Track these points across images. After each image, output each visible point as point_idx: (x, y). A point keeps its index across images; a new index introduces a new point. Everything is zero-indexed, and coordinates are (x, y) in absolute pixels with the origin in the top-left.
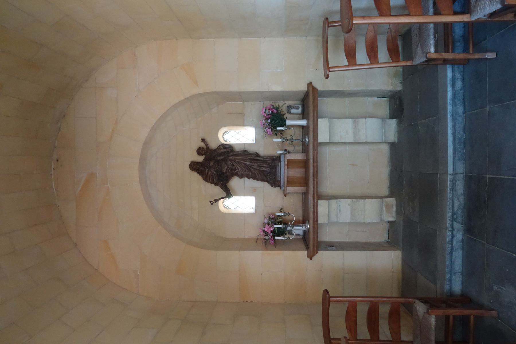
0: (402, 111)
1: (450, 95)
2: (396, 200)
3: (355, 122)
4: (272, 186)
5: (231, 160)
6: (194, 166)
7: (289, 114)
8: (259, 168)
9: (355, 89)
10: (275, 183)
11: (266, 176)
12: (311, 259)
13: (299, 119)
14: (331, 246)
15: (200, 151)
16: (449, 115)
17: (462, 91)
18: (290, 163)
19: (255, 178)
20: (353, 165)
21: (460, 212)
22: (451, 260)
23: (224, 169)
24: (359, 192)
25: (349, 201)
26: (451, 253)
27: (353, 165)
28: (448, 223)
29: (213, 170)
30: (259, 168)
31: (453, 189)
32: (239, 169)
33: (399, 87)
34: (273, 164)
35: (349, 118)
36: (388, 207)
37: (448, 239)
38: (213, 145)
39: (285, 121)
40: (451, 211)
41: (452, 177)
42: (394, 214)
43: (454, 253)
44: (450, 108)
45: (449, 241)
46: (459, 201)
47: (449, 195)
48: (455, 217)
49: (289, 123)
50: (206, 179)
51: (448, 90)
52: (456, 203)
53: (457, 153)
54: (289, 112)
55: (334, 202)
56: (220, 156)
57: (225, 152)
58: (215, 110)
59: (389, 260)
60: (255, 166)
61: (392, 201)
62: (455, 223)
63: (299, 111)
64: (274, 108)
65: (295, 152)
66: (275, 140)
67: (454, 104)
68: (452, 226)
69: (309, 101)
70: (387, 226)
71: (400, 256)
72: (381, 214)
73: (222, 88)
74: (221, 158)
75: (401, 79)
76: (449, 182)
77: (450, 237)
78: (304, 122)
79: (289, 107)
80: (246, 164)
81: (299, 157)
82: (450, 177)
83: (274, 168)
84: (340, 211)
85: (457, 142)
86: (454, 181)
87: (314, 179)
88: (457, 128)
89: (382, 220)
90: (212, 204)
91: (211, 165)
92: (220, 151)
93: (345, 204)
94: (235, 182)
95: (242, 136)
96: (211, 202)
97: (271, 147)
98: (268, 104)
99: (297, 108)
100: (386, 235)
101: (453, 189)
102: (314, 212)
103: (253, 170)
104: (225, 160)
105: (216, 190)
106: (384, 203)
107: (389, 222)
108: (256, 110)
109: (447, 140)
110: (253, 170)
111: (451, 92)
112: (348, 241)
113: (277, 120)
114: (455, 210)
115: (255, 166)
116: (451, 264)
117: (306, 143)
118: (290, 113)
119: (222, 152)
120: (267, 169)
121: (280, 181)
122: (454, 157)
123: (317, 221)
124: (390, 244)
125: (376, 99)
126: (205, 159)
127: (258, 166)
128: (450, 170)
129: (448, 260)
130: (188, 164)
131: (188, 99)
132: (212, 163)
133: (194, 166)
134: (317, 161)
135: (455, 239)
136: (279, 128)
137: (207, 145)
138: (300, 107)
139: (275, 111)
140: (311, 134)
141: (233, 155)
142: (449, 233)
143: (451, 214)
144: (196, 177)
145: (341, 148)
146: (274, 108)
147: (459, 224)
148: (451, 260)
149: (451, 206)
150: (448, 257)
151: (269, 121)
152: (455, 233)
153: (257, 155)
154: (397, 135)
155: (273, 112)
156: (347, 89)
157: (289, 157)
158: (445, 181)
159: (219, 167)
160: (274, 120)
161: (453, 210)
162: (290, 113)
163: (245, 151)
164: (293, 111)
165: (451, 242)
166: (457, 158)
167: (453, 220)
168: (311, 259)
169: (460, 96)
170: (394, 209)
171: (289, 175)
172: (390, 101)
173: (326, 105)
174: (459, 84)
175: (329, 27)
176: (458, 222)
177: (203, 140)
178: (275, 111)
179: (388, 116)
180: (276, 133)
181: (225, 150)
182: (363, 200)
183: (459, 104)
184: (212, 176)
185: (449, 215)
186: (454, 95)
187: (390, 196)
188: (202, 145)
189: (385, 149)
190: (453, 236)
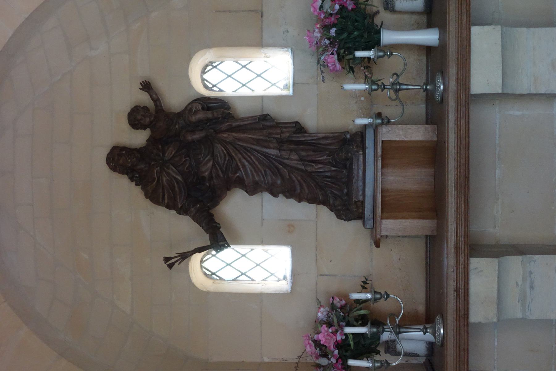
4: (339, 217)
5: (224, 143)
6: (120, 159)
10: (347, 208)
13: (418, 27)
15: (137, 116)
18: (391, 153)
19: (291, 193)
23: (206, 169)
29: (172, 171)
32: (247, 169)
34: (343, 155)
38: (175, 101)
39: (378, 32)
49: (388, 37)
55: (514, 263)
56: (193, 132)
57: (208, 120)
60: (293, 159)
66: (349, 87)
74: (197, 136)
81: (417, 134)
84: (532, 287)
87: (458, 197)
90: (171, 266)
91: (168, 156)
92: (194, 119)
94: (236, 206)
96: (167, 259)
102: (457, 290)
105: (183, 228)
110: (285, 172)
113: (357, 29)
115: (293, 159)
117: (438, 96)
120: (327, 168)
121: (363, 203)
123: (466, 315)
126: (151, 141)
127: (301, 159)
130: (103, 153)
132: (170, 152)
133: (120, 159)
134: (467, 147)
136: (359, 54)
137: (156, 100)
140: (452, 70)
141: (231, 129)
151: (333, 31)
153: (298, 127)
157: (388, 134)
171: (389, 186)
177: (147, 86)
180: (351, 67)
181: (209, 115)
188: (144, 99)
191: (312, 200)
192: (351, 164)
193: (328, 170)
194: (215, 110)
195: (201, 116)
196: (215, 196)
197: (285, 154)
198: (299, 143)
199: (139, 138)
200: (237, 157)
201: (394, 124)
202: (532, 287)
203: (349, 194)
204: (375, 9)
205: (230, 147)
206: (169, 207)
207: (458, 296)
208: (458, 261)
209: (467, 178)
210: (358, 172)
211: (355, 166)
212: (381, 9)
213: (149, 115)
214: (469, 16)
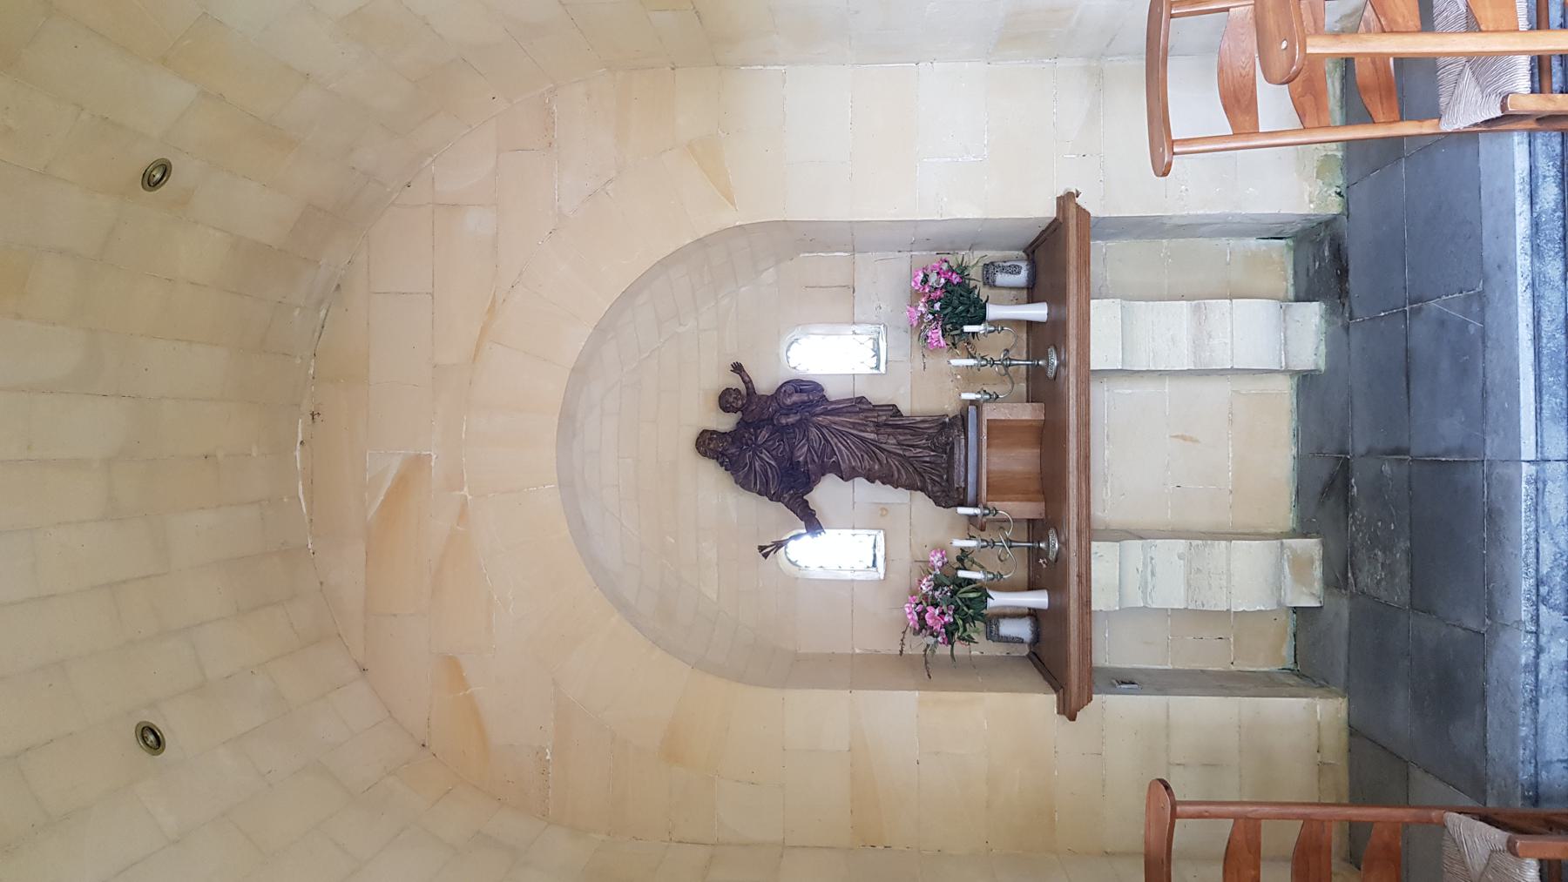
0: (1343, 274)
1: (1522, 225)
2: (1324, 545)
3: (1197, 309)
4: (938, 504)
5: (819, 427)
6: (708, 444)
7: (1020, 289)
8: (916, 453)
9: (1201, 212)
10: (947, 494)
11: (920, 474)
12: (1072, 718)
13: (1018, 302)
14: (1125, 681)
15: (726, 401)
16: (1522, 284)
17: (1559, 214)
18: (1001, 432)
19: (888, 479)
20: (1184, 438)
21: (1558, 576)
22: (1535, 721)
23: (801, 454)
24: (1202, 518)
25: (1181, 545)
26: (1535, 701)
27: (1184, 438)
28: (1525, 612)
29: (765, 456)
30: (916, 453)
31: (1537, 507)
32: (843, 453)
33: (1334, 207)
34: (943, 439)
35: (1182, 298)
36: (1300, 566)
37: (1525, 658)
38: (765, 383)
39: (984, 307)
40: (1532, 571)
41: (1533, 469)
42: (1317, 586)
43: (1541, 701)
44: (1523, 262)
45: (1526, 665)
46: (1556, 544)
47: (1525, 525)
48: (1544, 590)
49: (993, 312)
50: (745, 484)
51: (1518, 211)
52: (1547, 549)
53: (1546, 398)
54: (989, 282)
55: (1134, 546)
56: (787, 415)
57: (804, 402)
58: (769, 276)
59: (1308, 720)
60: (891, 443)
61: (1311, 547)
62: (1543, 609)
63: (1021, 278)
64: (951, 269)
65: (1012, 399)
66: (955, 362)
67: (1536, 252)
68: (1536, 619)
69: (1052, 255)
70: (1289, 623)
71: (1343, 714)
72: (1278, 587)
73: (802, 209)
74: (792, 419)
75: (1340, 182)
76: (1524, 485)
77: (1532, 653)
78: (1038, 312)
79: (989, 269)
80: (863, 440)
81: (1027, 413)
82: (1527, 470)
83: (948, 450)
84: (1153, 574)
85: (1545, 365)
86: (1539, 483)
87: (1079, 477)
88: (1544, 325)
89: (1279, 603)
90: (766, 556)
91: (760, 440)
92: (788, 401)
93: (1169, 552)
94: (827, 493)
95: (843, 353)
96: (761, 548)
97: (923, 384)
98: (931, 259)
99: (1015, 270)
100: (1287, 651)
101: (1537, 507)
102: (1079, 576)
103: (882, 456)
104: (802, 425)
105: (770, 515)
106: (1287, 552)
107: (1295, 610)
108: (888, 283)
109: (1516, 359)
110: (882, 456)
111: (1527, 214)
112: (1170, 667)
113: (961, 303)
114: (1544, 570)
115: (891, 443)
116: (1536, 734)
117: (1051, 373)
118: (993, 286)
119: (795, 403)
120: (926, 453)
121: (965, 489)
122: (1539, 412)
123: (1089, 603)
124: (1305, 673)
125: (1253, 242)
126: (742, 424)
127: (899, 444)
128: (1528, 450)
129: (1527, 721)
130: (691, 435)
131: (701, 243)
132: (764, 435)
133: (708, 444)
134: (1087, 425)
135: (1544, 657)
136: (967, 328)
137: (748, 383)
138: (1024, 265)
139: (956, 279)
140: (1072, 345)
141: (826, 413)
142: (1527, 641)
143: (1532, 581)
144: (711, 479)
145: (1146, 389)
146: (951, 269)
147: (1556, 614)
148: (1535, 721)
149: (1531, 559)
150: (1524, 715)
151: (937, 306)
152: (1543, 640)
153: (894, 410)
154: (1323, 348)
155: (948, 281)
156: (1179, 213)
157: (991, 412)
158: (1510, 486)
159: (777, 444)
160: (953, 306)
161: (1537, 570)
162: (993, 286)
163: (861, 400)
164: (1002, 279)
165: (1535, 667)
166: (1546, 413)
167: (1539, 600)
168: (1072, 718)
169: (1553, 229)
170: (1317, 572)
171: (992, 468)
172: (1295, 250)
173: (1108, 259)
174: (1550, 193)
175: (1172, 16)
176: (1554, 608)
177: (738, 368)
178: (956, 279)
179: (1291, 295)
180: (958, 341)
181: (804, 397)
182: (1223, 543)
183: (1552, 251)
184: (766, 475)
185: (1527, 584)
186: (1536, 225)
187: (1303, 531)
188: (735, 382)
189: (1285, 388)
190: (1539, 651)
191: (911, 487)
192: (952, 448)
193: (927, 455)
194: (806, 394)
195: (795, 398)
196: (809, 484)
197: (883, 438)
198: (898, 427)
199: (725, 422)
200: (833, 441)
201: (1003, 401)
202: (1153, 574)
203: (950, 480)
204: (972, 284)
205: (825, 431)
206: (760, 493)
207: (1080, 582)
208: (1079, 545)
209: (1087, 457)
210: (959, 455)
211: (956, 451)
212: (980, 285)
213: (740, 399)
214: (1088, 289)
